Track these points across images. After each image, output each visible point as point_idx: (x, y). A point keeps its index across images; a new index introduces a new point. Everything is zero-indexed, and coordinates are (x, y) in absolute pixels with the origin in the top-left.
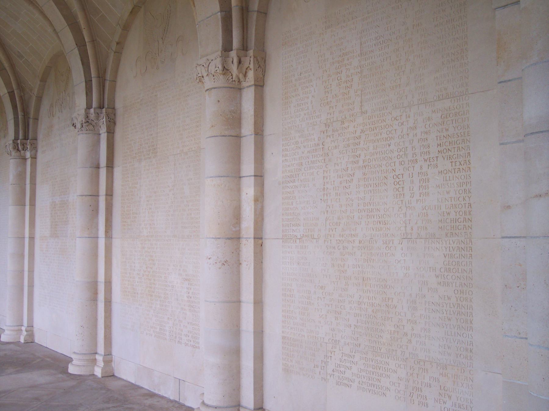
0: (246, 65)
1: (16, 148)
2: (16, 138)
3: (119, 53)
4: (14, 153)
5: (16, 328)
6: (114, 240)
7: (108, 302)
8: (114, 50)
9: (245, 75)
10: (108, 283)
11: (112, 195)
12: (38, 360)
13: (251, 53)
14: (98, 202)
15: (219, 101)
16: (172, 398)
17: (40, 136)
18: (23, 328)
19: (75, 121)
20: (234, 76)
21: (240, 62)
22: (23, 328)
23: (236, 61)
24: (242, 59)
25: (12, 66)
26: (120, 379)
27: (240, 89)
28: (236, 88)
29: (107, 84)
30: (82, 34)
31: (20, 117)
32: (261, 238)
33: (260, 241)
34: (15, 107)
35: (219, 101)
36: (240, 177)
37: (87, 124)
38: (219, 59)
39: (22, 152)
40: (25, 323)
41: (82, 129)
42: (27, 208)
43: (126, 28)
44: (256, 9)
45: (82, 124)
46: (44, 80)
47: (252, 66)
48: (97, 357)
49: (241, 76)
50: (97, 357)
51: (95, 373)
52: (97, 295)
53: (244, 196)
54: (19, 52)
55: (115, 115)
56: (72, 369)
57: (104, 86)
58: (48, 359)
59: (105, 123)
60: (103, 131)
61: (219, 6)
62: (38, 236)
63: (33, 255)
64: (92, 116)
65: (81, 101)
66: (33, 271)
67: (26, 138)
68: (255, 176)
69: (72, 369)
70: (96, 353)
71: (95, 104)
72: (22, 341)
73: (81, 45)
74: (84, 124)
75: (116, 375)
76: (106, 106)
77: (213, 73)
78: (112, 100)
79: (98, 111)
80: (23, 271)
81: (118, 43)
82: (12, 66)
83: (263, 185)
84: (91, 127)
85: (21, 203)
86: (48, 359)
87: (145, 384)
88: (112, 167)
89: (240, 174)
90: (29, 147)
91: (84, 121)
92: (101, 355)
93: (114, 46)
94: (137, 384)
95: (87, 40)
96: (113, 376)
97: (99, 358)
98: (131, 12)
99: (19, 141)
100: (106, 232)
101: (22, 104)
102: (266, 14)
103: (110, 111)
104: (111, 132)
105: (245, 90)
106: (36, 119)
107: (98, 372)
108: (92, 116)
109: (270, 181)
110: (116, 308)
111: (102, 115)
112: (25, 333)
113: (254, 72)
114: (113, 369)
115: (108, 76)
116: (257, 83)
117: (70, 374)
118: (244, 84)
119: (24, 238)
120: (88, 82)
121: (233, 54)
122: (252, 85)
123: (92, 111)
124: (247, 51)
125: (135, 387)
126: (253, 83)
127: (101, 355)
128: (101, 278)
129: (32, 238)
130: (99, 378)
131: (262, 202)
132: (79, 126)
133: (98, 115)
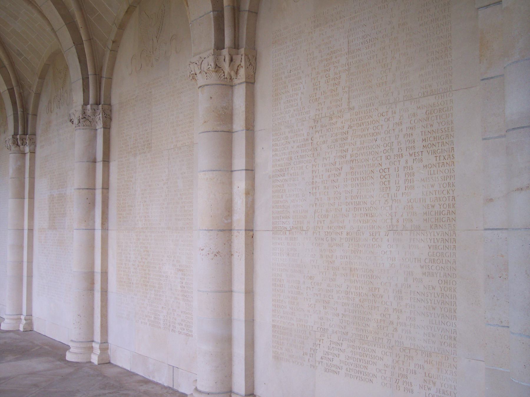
0: (238, 63)
1: (15, 143)
2: (16, 134)
3: (115, 51)
4: (13, 148)
5: (16, 317)
6: (110, 232)
7: (104, 292)
8: (110, 48)
9: (237, 73)
10: (105, 274)
11: (108, 189)
12: (37, 348)
13: (242, 51)
14: (94, 195)
15: (211, 98)
16: (166, 385)
17: (39, 132)
18: (23, 317)
19: (73, 117)
20: (226, 74)
21: (231, 60)
22: (23, 317)
23: (227, 59)
24: (234, 57)
25: (12, 64)
26: (116, 366)
27: (232, 86)
28: (228, 85)
29: (104, 81)
30: (80, 33)
31: (19, 113)
32: (252, 230)
33: (251, 233)
34: (14, 104)
35: (211, 98)
36: (232, 171)
37: (84, 119)
38: (211, 57)
39: (22, 147)
40: (24, 312)
41: (79, 124)
42: (26, 201)
43: (122, 27)
44: (247, 8)
45: (79, 120)
46: (42, 77)
47: (243, 64)
48: (94, 345)
49: (233, 73)
50: (94, 345)
51: (92, 361)
52: (94, 285)
53: (235, 190)
54: (18, 50)
55: (111, 111)
56: (69, 357)
57: (100, 83)
58: (46, 347)
59: (101, 119)
60: (100, 126)
61: (211, 6)
62: (36, 227)
63: (32, 246)
64: (89, 112)
65: (78, 98)
66: (32, 262)
67: (25, 133)
68: (246, 170)
69: (69, 357)
70: (93, 341)
71: (91, 101)
72: (21, 329)
73: (78, 43)
74: (81, 120)
75: (112, 362)
76: (102, 102)
77: (205, 70)
78: (109, 97)
79: (95, 107)
80: (22, 261)
81: (113, 42)
82: (12, 64)
83: (253, 179)
84: (88, 123)
85: (20, 196)
86: (46, 347)
87: (140, 371)
88: (108, 162)
89: (231, 168)
90: (28, 142)
91: (81, 116)
92: (97, 343)
93: (110, 45)
94: (133, 371)
95: (84, 39)
96: (109, 363)
97: (96, 346)
98: (127, 12)
99: (18, 137)
100: (103, 224)
101: (21, 100)
102: (257, 13)
103: (106, 107)
104: (107, 128)
105: (237, 87)
106: (35, 115)
107: (95, 359)
108: (89, 112)
109: (260, 175)
110: (112, 297)
111: (98, 112)
112: (24, 322)
113: (245, 69)
114: (109, 357)
115: (105, 74)
116: (248, 81)
117: (68, 361)
118: (236, 81)
119: (23, 230)
120: (85, 79)
121: (225, 52)
122: (243, 83)
123: (89, 107)
124: (238, 49)
125: (130, 374)
126: (244, 80)
127: (97, 343)
128: (98, 268)
129: (31, 230)
130: (96, 365)
131: (253, 195)
132: (76, 121)
133: (94, 111)
